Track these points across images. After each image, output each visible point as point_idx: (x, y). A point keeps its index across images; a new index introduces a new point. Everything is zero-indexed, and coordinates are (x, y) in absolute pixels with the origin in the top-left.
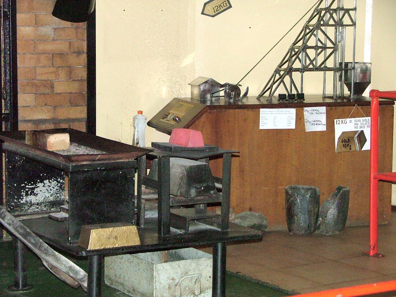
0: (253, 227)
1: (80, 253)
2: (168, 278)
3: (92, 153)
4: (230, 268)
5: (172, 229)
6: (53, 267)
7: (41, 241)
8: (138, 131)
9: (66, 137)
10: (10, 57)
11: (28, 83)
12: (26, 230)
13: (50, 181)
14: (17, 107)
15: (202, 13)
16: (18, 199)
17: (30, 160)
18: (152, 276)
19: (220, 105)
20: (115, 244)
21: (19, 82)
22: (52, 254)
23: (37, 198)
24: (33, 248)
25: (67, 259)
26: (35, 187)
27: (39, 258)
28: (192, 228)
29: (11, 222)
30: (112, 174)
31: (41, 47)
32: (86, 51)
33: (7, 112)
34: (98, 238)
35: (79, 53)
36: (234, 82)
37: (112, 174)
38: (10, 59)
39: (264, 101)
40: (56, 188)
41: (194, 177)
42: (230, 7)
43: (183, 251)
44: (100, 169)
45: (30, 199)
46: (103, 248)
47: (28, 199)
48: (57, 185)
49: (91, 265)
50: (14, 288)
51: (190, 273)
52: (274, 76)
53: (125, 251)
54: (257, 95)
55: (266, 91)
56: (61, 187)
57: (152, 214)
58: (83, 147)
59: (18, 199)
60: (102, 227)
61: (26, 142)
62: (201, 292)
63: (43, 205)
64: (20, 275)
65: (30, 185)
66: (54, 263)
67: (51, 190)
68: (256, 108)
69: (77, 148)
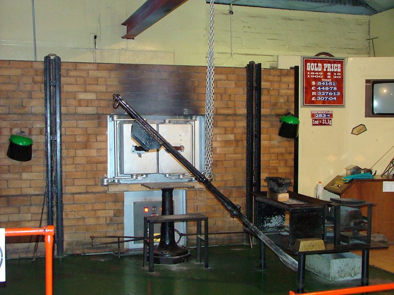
0: (380, 242)
2: (338, 267)
4: (371, 263)
5: (341, 243)
6: (284, 261)
7: (279, 248)
8: (319, 192)
9: (287, 195)
11: (265, 168)
12: (271, 242)
15: (352, 133)
16: (262, 225)
17: (269, 206)
18: (330, 265)
19: (261, 187)
20: (312, 249)
22: (284, 255)
24: (275, 251)
25: (291, 258)
27: (278, 257)
28: (351, 242)
29: (264, 238)
30: (311, 214)
31: (272, 151)
32: (293, 152)
33: (255, 182)
34: (304, 245)
35: (290, 153)
36: (369, 168)
37: (311, 214)
39: (384, 177)
40: (281, 220)
41: (353, 216)
42: (366, 130)
43: (345, 254)
44: (305, 211)
47: (267, 225)
49: (300, 258)
50: (259, 268)
51: (349, 265)
52: (390, 165)
53: (317, 253)
54: (381, 174)
55: (386, 172)
56: (283, 219)
57: (330, 234)
58: (295, 200)
59: (262, 225)
60: (306, 240)
61: (267, 197)
62: (355, 275)
63: (275, 228)
66: (285, 259)
68: (381, 181)
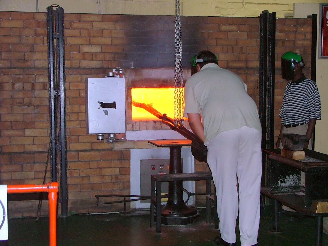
1: (312, 215)
3: (317, 162)
10: (270, 111)
13: (293, 175)
14: (274, 136)
16: (276, 184)
21: (275, 124)
23: (286, 184)
26: (285, 179)
38: (270, 112)
40: (296, 179)
45: (282, 184)
46: (324, 212)
47: (281, 185)
48: (297, 178)
56: (298, 179)
58: (312, 158)
61: (281, 155)
64: (276, 223)
65: (283, 177)
67: (293, 180)
69: (308, 158)
